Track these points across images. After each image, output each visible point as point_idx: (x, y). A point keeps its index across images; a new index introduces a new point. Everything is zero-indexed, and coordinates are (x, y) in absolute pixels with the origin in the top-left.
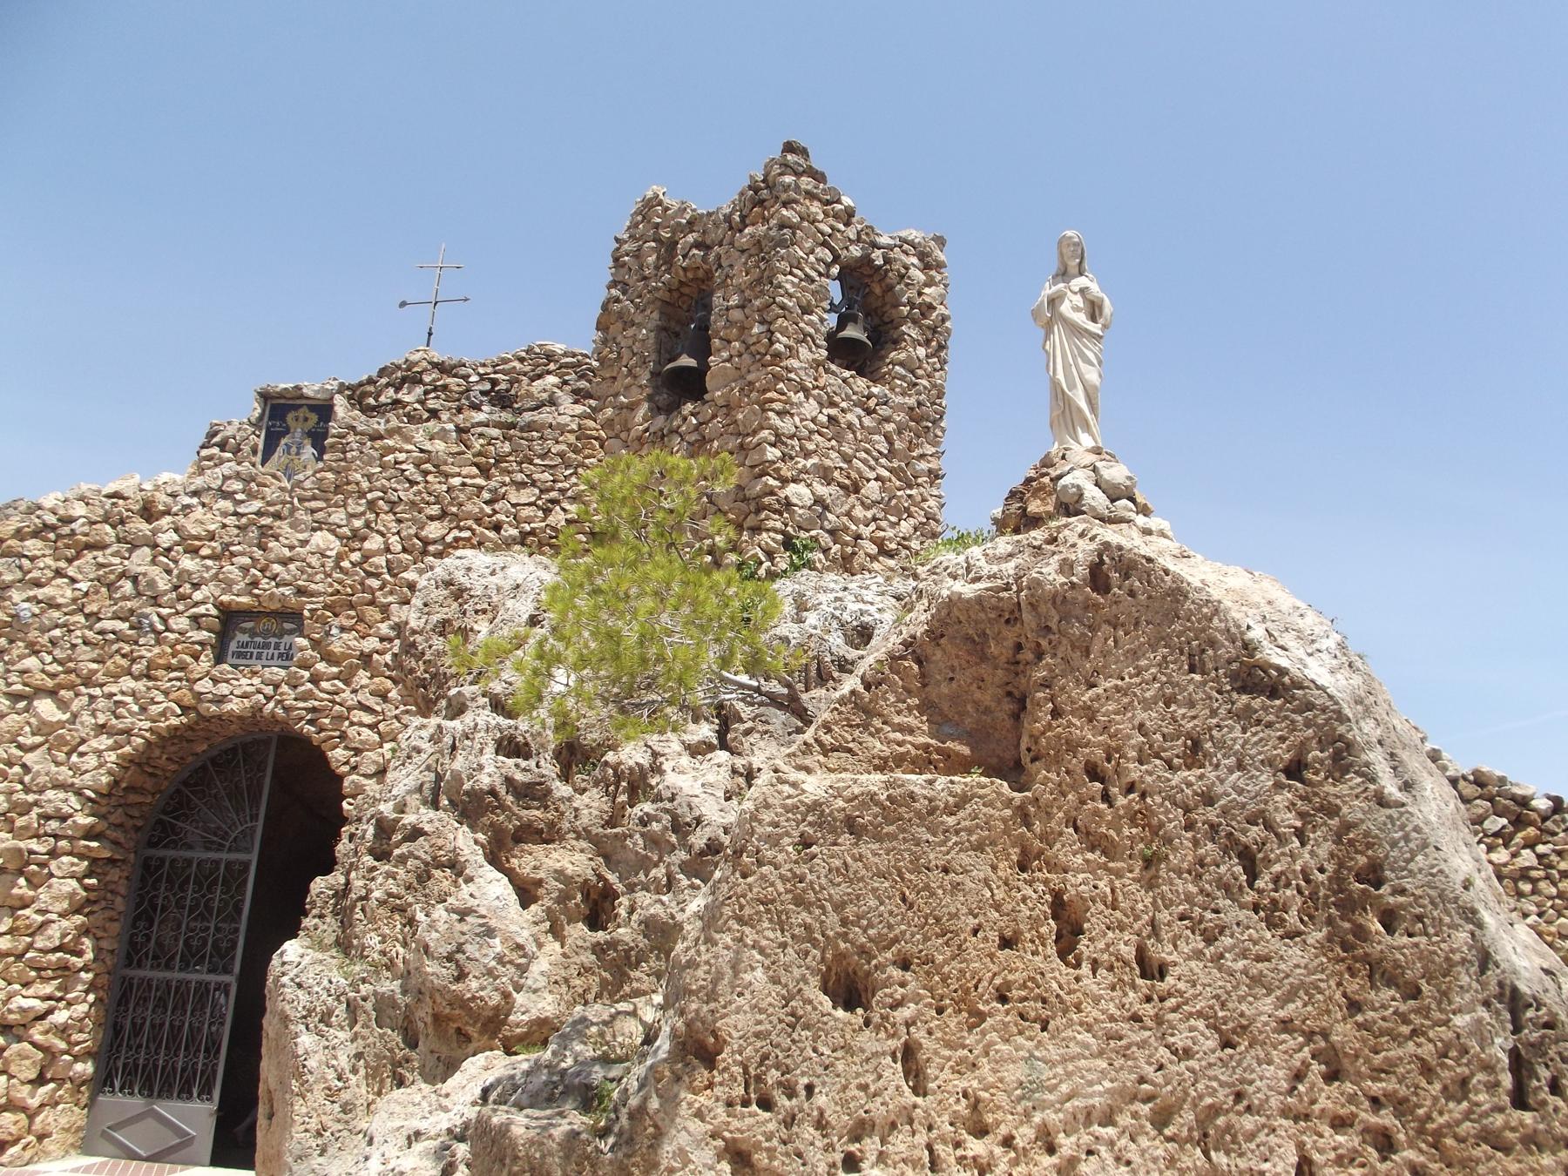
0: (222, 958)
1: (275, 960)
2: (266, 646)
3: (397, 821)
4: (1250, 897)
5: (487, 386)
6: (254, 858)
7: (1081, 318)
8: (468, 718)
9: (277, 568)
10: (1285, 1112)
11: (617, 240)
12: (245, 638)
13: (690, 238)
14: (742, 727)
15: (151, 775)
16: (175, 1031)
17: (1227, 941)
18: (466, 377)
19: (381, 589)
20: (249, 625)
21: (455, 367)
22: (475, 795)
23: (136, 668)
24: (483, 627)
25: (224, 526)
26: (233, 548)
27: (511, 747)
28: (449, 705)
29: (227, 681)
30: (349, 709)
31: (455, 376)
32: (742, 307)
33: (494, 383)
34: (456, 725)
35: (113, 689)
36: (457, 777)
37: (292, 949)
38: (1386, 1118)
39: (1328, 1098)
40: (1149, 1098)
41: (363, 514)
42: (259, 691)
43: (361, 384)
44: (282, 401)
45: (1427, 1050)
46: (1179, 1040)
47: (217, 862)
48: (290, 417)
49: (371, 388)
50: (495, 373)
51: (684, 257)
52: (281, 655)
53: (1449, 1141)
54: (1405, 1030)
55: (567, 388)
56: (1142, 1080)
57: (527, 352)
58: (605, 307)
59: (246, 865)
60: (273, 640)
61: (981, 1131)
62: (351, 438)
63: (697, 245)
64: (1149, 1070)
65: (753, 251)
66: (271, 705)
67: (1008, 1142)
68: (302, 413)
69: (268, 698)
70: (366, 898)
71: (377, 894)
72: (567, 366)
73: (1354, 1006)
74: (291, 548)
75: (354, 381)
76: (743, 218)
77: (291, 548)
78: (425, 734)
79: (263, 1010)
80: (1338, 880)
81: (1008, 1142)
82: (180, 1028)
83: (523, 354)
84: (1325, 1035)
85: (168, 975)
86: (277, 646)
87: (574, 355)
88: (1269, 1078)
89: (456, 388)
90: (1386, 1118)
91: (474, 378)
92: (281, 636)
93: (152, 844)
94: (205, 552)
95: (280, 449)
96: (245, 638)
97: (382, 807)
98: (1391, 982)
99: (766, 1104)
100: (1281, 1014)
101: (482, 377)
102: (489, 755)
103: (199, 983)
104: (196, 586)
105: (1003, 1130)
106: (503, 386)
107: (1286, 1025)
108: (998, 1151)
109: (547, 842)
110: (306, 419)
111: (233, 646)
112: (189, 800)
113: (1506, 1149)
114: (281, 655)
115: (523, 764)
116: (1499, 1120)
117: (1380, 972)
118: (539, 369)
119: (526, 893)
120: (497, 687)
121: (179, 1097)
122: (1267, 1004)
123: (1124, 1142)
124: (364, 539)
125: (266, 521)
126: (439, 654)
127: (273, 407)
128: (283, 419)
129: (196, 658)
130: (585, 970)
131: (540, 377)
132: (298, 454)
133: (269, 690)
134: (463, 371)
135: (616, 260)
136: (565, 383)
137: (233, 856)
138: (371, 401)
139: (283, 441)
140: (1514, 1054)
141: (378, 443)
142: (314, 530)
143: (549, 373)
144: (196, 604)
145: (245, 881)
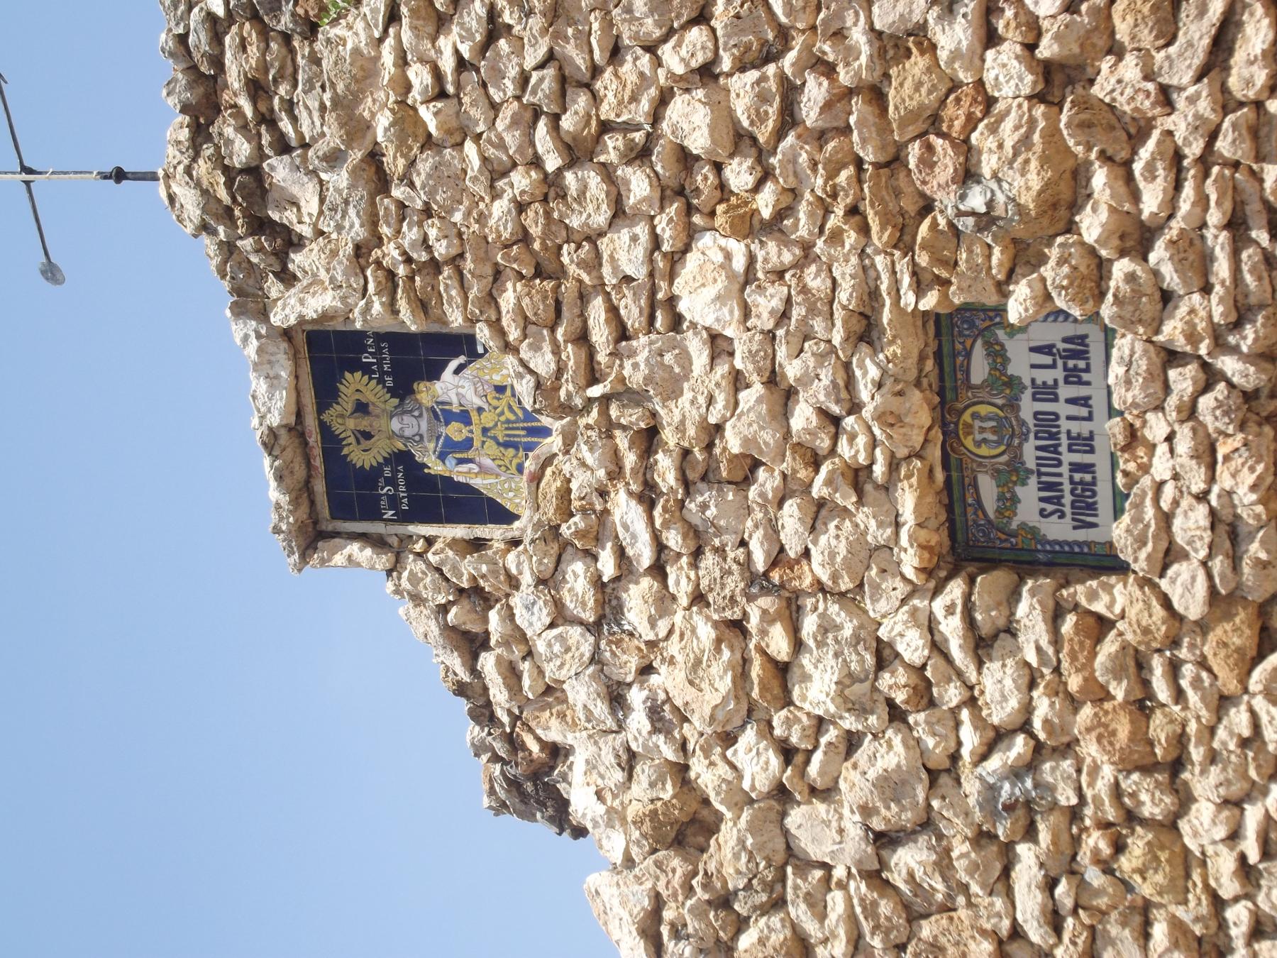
2: (1047, 424)
9: (802, 417)
12: (1029, 495)
19: (829, 70)
20: (988, 489)
23: (1152, 804)
25: (699, 598)
26: (760, 563)
29: (1166, 519)
30: (1227, 104)
35: (1224, 866)
41: (607, 172)
42: (1190, 412)
44: (320, 486)
48: (362, 457)
52: (1073, 377)
60: (1028, 408)
62: (391, 253)
66: (1229, 365)
68: (344, 423)
69: (1210, 377)
74: (738, 381)
77: (738, 381)
86: (1046, 392)
92: (1013, 384)
94: (779, 644)
95: (461, 474)
96: (1029, 495)
104: (884, 656)
110: (362, 408)
111: (1059, 530)
114: (1073, 377)
124: (686, 159)
125: (666, 471)
127: (342, 509)
128: (370, 478)
129: (1102, 625)
132: (464, 417)
133: (1183, 380)
134: (199, 40)
139: (436, 468)
141: (394, 163)
142: (676, 322)
144: (938, 647)
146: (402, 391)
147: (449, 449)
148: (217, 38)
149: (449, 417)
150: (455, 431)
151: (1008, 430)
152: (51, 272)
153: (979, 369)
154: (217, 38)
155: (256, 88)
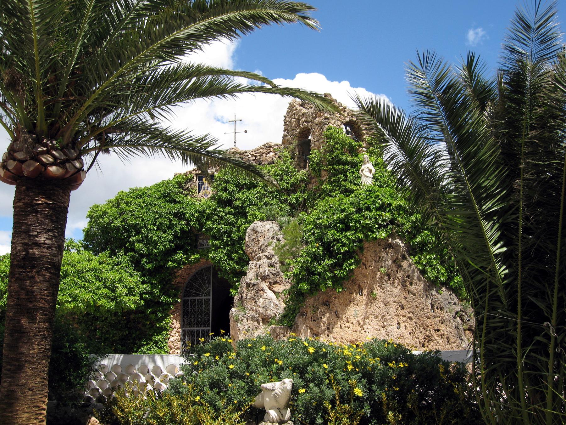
1: (231, 312)
3: (250, 283)
4: (389, 282)
5: (254, 158)
6: (211, 297)
8: (262, 261)
10: (395, 315)
11: (284, 116)
13: (303, 119)
15: (183, 278)
17: (385, 289)
20: (202, 237)
21: (244, 153)
22: (265, 276)
24: (262, 240)
27: (271, 265)
28: (257, 258)
32: (318, 141)
33: (256, 157)
34: (259, 262)
36: (261, 273)
37: (233, 309)
38: (411, 315)
39: (402, 312)
40: (374, 315)
45: (417, 304)
46: (378, 306)
47: (202, 299)
51: (302, 125)
53: (420, 318)
54: (414, 301)
55: (277, 156)
56: (372, 312)
57: (264, 146)
58: (283, 137)
59: (209, 299)
61: (348, 322)
63: (305, 121)
64: (373, 311)
67: (352, 323)
70: (246, 298)
71: (248, 297)
73: (406, 298)
76: (316, 115)
78: (254, 265)
79: (229, 321)
80: (403, 278)
81: (352, 323)
83: (263, 147)
84: (401, 303)
85: (194, 328)
88: (392, 310)
90: (411, 315)
91: (250, 156)
93: (185, 296)
95: (202, 189)
96: (201, 241)
97: (247, 280)
98: (411, 293)
99: (314, 321)
100: (394, 300)
101: (252, 155)
102: (267, 269)
105: (351, 322)
106: (258, 157)
107: (395, 302)
108: (351, 325)
109: (280, 284)
112: (192, 284)
113: (429, 318)
115: (274, 269)
116: (428, 314)
117: (409, 292)
119: (277, 294)
120: (267, 254)
122: (392, 299)
123: (370, 322)
126: (254, 246)
131: (268, 153)
132: (207, 189)
134: (246, 154)
135: (285, 123)
136: (276, 154)
137: (206, 297)
139: (203, 187)
140: (431, 303)
143: (271, 152)
145: (209, 304)
147: (204, 188)
150: (206, 189)
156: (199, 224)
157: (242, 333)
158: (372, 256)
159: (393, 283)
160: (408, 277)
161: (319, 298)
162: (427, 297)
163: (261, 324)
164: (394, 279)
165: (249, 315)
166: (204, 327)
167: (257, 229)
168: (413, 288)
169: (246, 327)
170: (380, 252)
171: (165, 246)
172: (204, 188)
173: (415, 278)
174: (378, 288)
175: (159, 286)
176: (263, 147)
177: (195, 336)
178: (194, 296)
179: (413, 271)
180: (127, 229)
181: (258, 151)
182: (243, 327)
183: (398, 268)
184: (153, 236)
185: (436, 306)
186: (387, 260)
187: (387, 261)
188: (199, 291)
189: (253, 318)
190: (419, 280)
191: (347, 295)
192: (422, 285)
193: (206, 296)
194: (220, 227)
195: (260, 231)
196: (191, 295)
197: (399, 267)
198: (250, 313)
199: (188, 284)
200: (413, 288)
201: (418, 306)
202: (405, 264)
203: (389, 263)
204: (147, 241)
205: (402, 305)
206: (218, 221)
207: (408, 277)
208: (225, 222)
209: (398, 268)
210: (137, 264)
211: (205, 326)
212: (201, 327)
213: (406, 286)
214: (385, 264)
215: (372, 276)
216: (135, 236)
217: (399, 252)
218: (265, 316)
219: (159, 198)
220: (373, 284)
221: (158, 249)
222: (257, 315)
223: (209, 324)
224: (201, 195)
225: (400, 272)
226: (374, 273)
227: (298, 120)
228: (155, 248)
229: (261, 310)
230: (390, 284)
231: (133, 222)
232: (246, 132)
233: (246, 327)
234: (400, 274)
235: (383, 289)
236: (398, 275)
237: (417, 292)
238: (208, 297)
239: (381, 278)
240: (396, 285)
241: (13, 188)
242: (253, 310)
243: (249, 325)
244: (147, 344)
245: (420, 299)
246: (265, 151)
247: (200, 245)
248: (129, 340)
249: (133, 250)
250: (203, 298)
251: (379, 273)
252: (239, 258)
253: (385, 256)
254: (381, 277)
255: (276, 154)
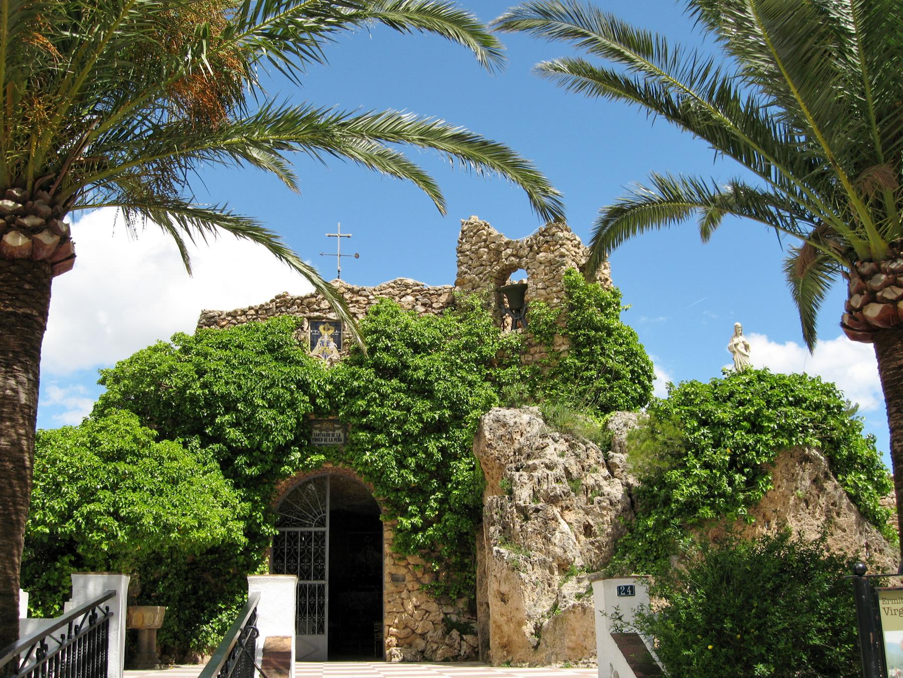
0: (305, 573)
2: (329, 435)
4: (807, 511)
6: (327, 529)
7: (743, 351)
12: (317, 432)
13: (509, 251)
14: (620, 470)
16: (312, 607)
17: (803, 522)
18: (367, 296)
20: (318, 426)
31: (361, 295)
43: (306, 297)
45: (848, 544)
49: (314, 300)
50: (381, 294)
60: (331, 432)
65: (547, 264)
72: (416, 291)
75: (303, 295)
80: (827, 506)
82: (314, 604)
83: (393, 285)
86: (333, 435)
87: (418, 285)
89: (363, 302)
92: (334, 431)
95: (318, 344)
96: (317, 432)
98: (840, 528)
103: (310, 586)
109: (570, 510)
114: (335, 439)
118: (403, 293)
121: (318, 633)
128: (317, 328)
130: (589, 550)
131: (403, 296)
132: (327, 346)
134: (364, 293)
137: (317, 529)
138: (315, 306)
139: (319, 340)
143: (408, 294)
145: (324, 541)
146: (331, 336)
147: (323, 342)
148: (365, 296)
149: (328, 343)
150: (325, 344)
151: (327, 429)
152: (339, 271)
153: (336, 426)
154: (365, 296)
155: (357, 301)
156: (330, 404)
157: (529, 588)
158: (783, 471)
159: (814, 513)
160: (834, 504)
161: (707, 533)
162: (861, 533)
163: (556, 573)
164: (815, 507)
165: (536, 558)
166: (314, 579)
167: (505, 420)
168: (841, 520)
169: (533, 578)
170: (794, 466)
171: (285, 437)
172: (323, 342)
173: (844, 506)
174: (792, 519)
175: (261, 506)
176: (393, 285)
177: (305, 596)
178: (295, 526)
179: (841, 497)
180: (211, 401)
181: (387, 291)
182: (528, 578)
183: (820, 492)
184: (265, 416)
185: (873, 548)
186: (803, 479)
187: (804, 480)
188: (306, 518)
189: (543, 564)
190: (850, 510)
191: (750, 529)
192: (854, 517)
193: (318, 526)
194: (384, 410)
195: (511, 423)
196: (288, 524)
197: (822, 489)
198: (537, 555)
199: (283, 504)
200: (841, 520)
201: (850, 546)
202: (829, 486)
203: (808, 483)
204: (248, 424)
205: (828, 545)
206: (378, 401)
207: (834, 504)
208: (392, 404)
209: (820, 492)
210: (227, 466)
211: (316, 579)
212: (308, 579)
213: (832, 517)
214: (801, 484)
215: (782, 502)
216: (224, 415)
217: (819, 469)
218: (563, 561)
219: (263, 353)
220: (785, 513)
221: (273, 441)
222: (551, 559)
223: (324, 575)
224: (317, 354)
225: (823, 497)
226: (786, 497)
227: (498, 253)
228: (267, 439)
229: (559, 551)
230: (809, 514)
231: (224, 389)
232: (357, 256)
233: (533, 578)
234: (823, 499)
235: (799, 521)
236: (821, 502)
237: (848, 526)
238: (322, 529)
239: (796, 505)
240: (817, 515)
241: (871, 346)
242: (541, 551)
243: (537, 575)
244: (226, 609)
245: (851, 537)
246: (398, 292)
247: (316, 440)
248: (189, 602)
249: (218, 437)
250: (313, 529)
251: (792, 498)
252: (418, 465)
253: (801, 473)
254: (796, 504)
255: (417, 300)
